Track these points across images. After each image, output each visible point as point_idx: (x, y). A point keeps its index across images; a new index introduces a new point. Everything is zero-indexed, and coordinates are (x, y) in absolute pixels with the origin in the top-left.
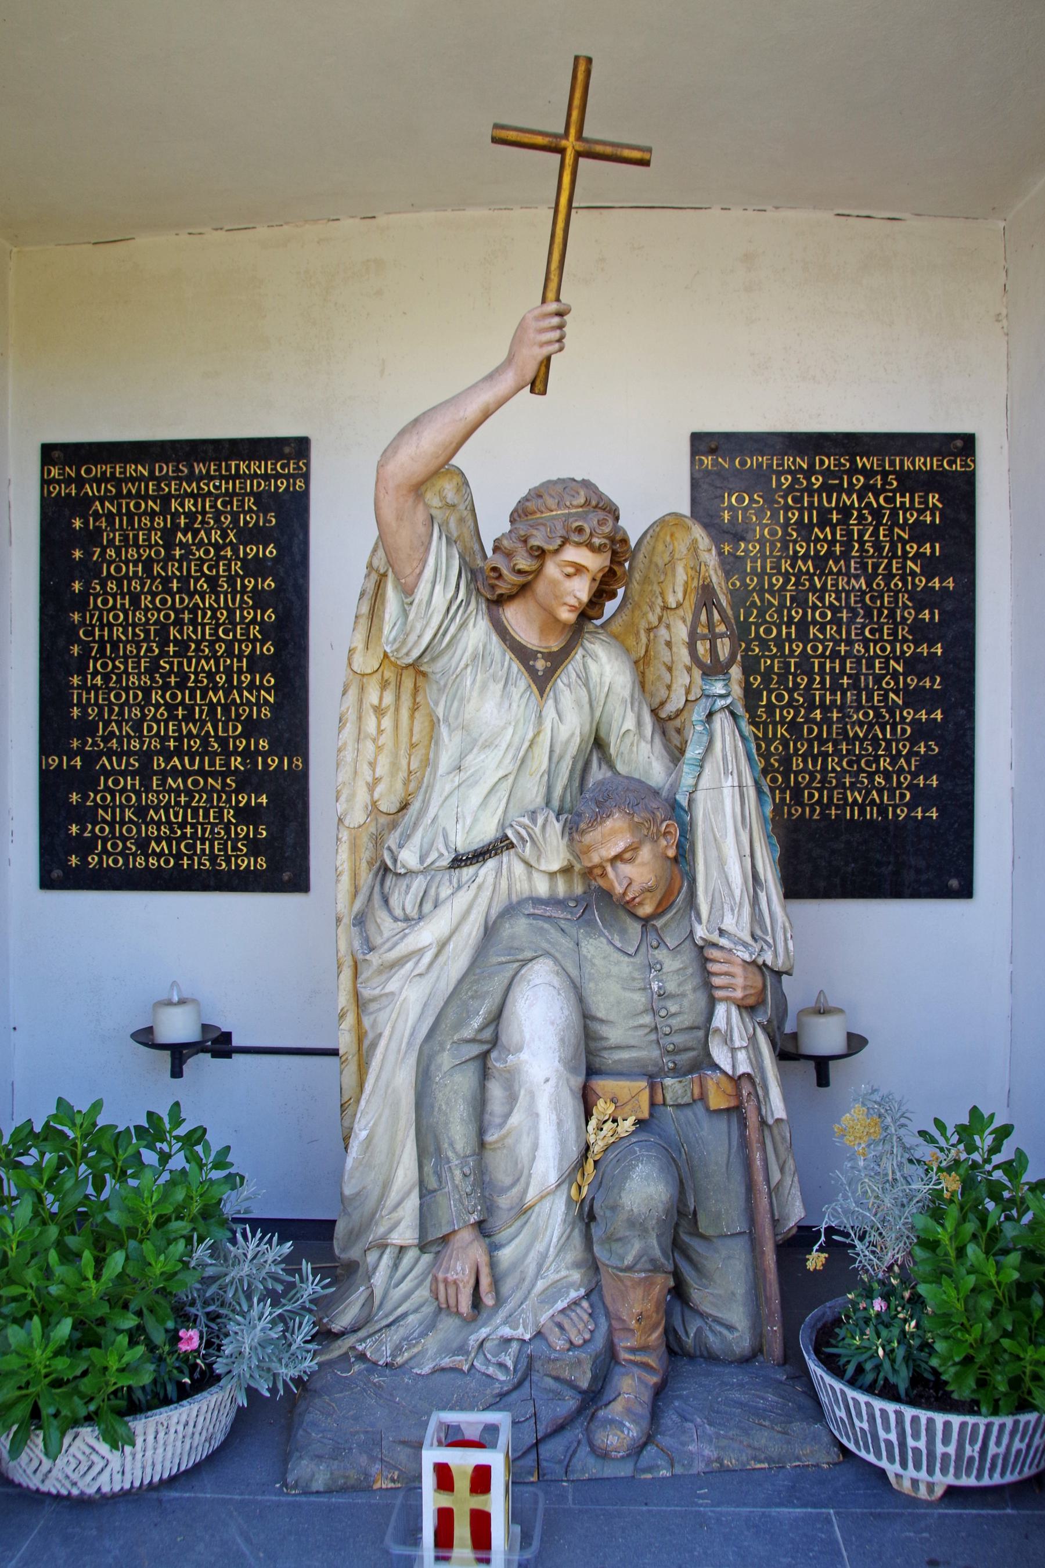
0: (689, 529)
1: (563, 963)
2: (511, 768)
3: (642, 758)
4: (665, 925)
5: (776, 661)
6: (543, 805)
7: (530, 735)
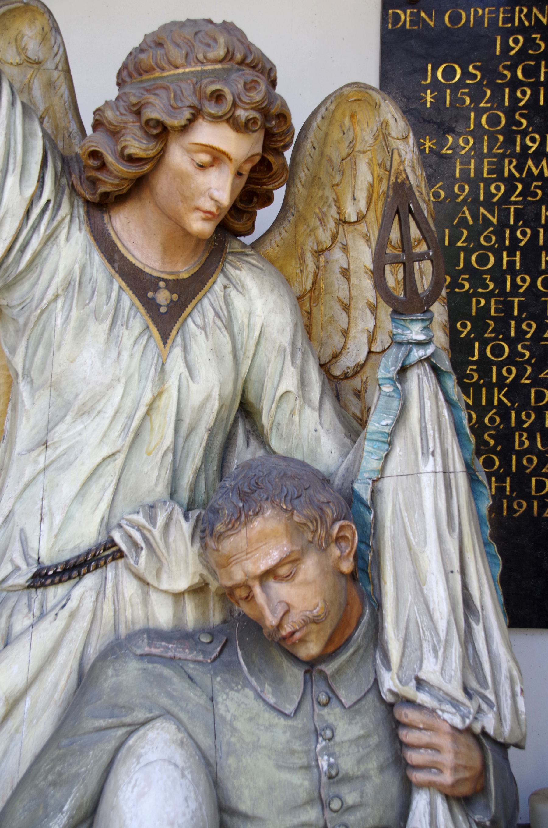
0: (377, 107)
1: (190, 727)
2: (119, 443)
3: (306, 430)
4: (338, 671)
5: (493, 301)
6: (166, 496)
7: (148, 397)
